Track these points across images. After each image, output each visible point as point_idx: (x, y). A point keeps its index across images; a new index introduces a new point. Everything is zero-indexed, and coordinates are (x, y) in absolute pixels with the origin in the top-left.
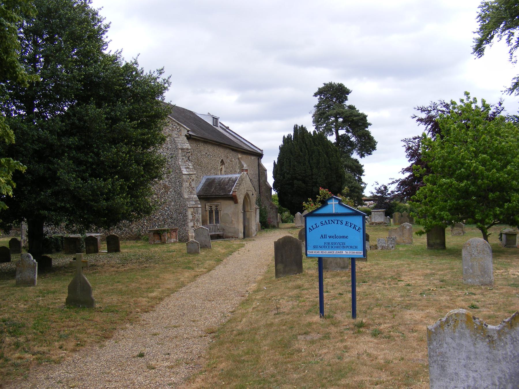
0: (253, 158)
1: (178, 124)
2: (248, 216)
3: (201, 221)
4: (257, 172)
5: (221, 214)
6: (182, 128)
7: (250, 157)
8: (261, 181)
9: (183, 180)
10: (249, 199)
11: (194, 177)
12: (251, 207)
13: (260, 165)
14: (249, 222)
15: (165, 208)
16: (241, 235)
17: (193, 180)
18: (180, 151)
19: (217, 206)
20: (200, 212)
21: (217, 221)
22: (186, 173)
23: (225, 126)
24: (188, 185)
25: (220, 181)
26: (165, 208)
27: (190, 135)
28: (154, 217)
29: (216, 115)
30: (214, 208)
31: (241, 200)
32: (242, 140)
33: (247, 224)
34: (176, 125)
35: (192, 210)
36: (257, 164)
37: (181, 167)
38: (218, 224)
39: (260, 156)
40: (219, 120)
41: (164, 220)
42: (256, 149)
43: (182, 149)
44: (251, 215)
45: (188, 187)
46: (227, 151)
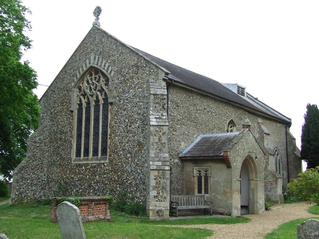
0: (279, 125)
1: (156, 66)
2: (252, 186)
3: (168, 188)
4: (285, 141)
5: (211, 181)
6: (160, 71)
7: (274, 124)
8: (289, 150)
9: (150, 133)
10: (254, 164)
11: (165, 129)
12: (256, 174)
13: (287, 134)
14: (253, 194)
15: (139, 171)
16: (236, 212)
17: (164, 134)
18: (152, 97)
19: (206, 171)
20: (168, 176)
21: (206, 192)
22: (154, 123)
23: (254, 98)
24: (157, 140)
25: (215, 141)
26: (139, 171)
27: (169, 79)
28: (127, 182)
29: (242, 84)
30: (203, 174)
31: (237, 163)
32: (270, 109)
33: (251, 197)
34: (154, 67)
35: (156, 173)
36: (284, 132)
37: (151, 117)
38: (207, 195)
39: (287, 124)
40: (246, 91)
41: (137, 185)
42: (276, 113)
43: (154, 95)
44: (256, 185)
45: (156, 143)
46: (240, 112)
